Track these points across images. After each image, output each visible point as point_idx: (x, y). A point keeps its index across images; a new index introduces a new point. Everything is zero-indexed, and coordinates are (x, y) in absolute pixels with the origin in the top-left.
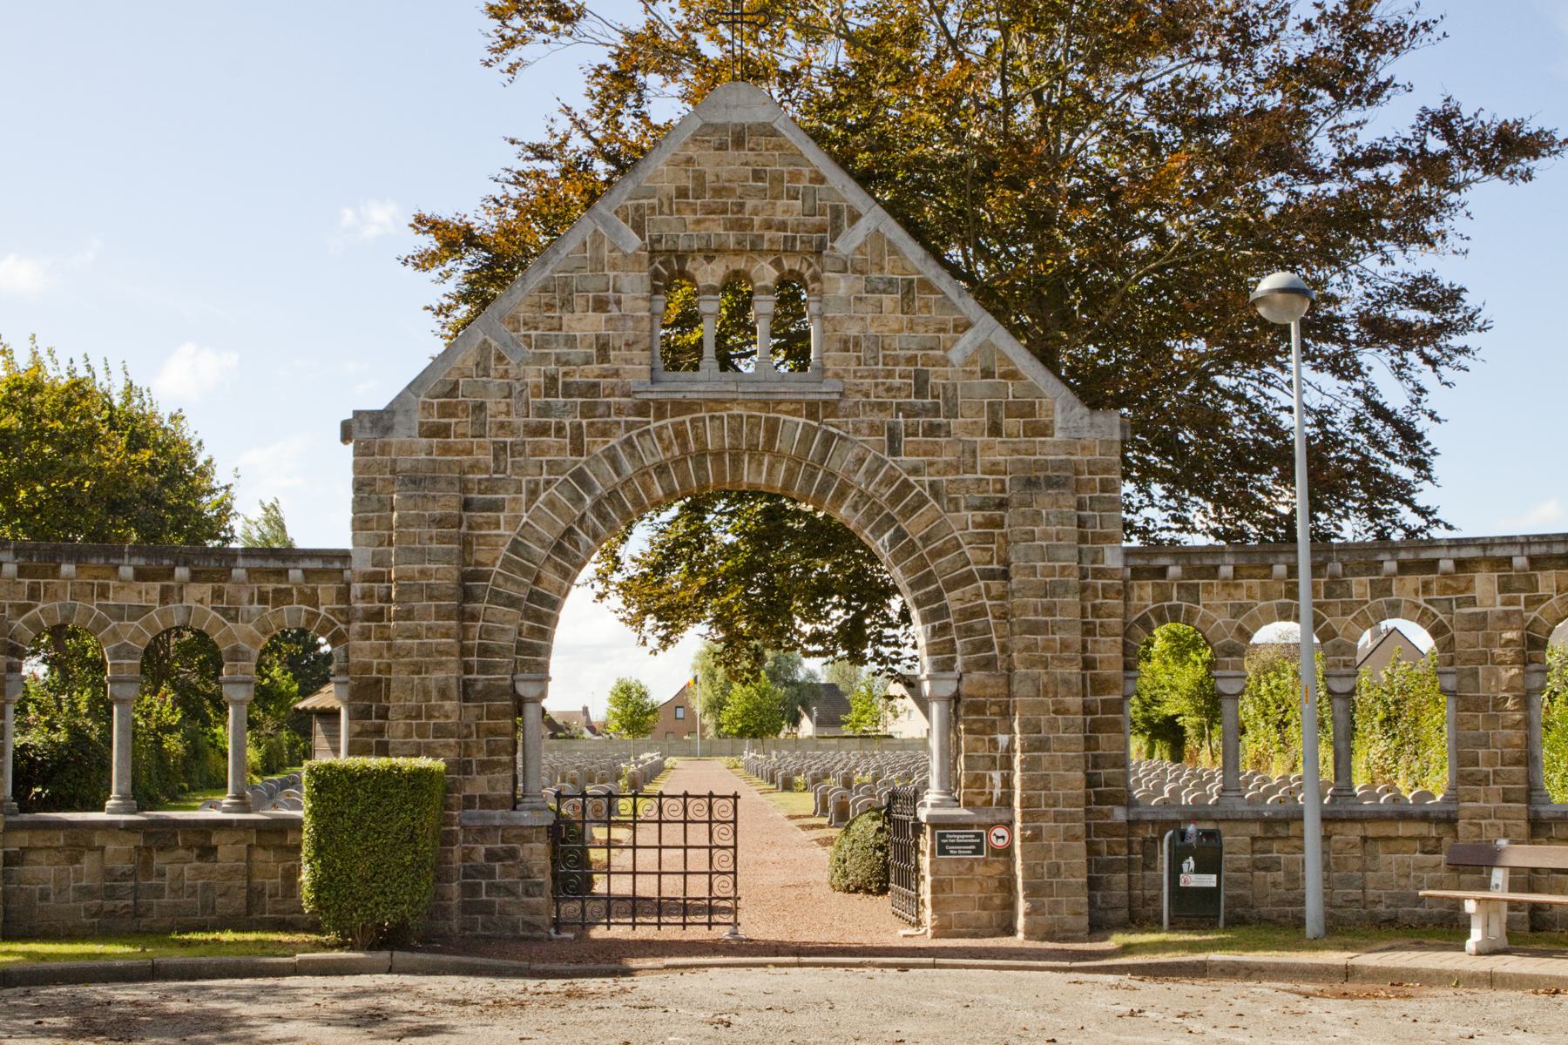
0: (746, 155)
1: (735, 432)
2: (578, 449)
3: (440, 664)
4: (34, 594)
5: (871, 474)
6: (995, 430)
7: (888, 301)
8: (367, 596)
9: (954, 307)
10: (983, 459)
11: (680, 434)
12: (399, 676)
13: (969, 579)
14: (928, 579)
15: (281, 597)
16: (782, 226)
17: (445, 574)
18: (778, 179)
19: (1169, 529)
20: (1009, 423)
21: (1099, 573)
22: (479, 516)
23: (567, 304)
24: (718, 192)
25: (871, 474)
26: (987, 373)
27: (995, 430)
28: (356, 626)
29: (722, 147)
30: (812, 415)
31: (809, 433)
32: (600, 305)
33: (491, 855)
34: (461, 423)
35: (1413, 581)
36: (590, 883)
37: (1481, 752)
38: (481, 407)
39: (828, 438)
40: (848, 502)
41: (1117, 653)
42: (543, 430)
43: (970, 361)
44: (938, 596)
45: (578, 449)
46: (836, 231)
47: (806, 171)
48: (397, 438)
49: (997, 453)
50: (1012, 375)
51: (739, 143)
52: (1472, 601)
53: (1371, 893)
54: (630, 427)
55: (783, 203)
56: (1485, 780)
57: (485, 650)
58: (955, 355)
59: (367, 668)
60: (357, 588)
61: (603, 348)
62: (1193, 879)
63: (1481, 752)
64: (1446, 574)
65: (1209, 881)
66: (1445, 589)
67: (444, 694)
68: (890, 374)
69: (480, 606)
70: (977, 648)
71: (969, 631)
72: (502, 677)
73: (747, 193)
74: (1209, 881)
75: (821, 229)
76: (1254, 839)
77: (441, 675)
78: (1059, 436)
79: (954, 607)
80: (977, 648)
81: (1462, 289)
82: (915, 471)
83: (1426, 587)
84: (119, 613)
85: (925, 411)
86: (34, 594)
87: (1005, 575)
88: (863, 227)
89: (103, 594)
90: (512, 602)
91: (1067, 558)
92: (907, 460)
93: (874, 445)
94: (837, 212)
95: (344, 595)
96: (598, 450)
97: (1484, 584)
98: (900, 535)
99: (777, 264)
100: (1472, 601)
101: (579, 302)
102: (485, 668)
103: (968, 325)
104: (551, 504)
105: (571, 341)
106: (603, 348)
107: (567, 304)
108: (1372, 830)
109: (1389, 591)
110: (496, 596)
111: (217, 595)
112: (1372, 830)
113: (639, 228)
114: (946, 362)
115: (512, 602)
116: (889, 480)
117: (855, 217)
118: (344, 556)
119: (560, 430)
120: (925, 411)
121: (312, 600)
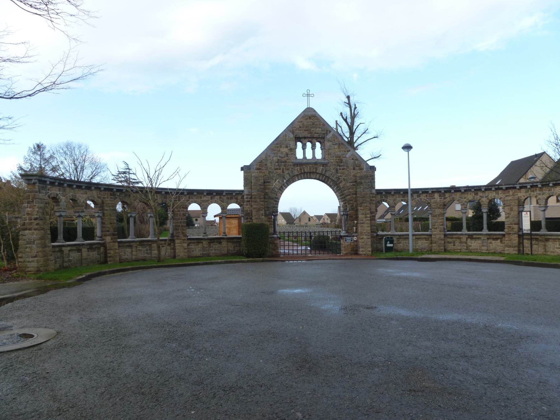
0: (311, 120)
4: (189, 198)
6: (354, 169)
7: (336, 147)
8: (247, 198)
11: (301, 169)
12: (254, 213)
14: (343, 194)
18: (317, 125)
19: (29, 262)
24: (307, 127)
26: (353, 159)
28: (245, 203)
30: (323, 166)
32: (287, 147)
35: (425, 195)
38: (266, 165)
39: (326, 171)
43: (350, 157)
45: (283, 172)
46: (327, 134)
48: (252, 170)
51: (310, 118)
52: (434, 198)
53: (417, 247)
54: (292, 168)
55: (318, 129)
56: (436, 228)
58: (347, 156)
59: (247, 211)
60: (245, 197)
62: (389, 245)
65: (392, 245)
66: (430, 196)
67: (262, 215)
73: (311, 128)
74: (392, 245)
75: (324, 134)
81: (242, 169)
83: (426, 196)
87: (356, 194)
89: (201, 198)
94: (327, 131)
95: (243, 198)
100: (434, 198)
102: (268, 210)
105: (282, 153)
107: (281, 147)
108: (417, 237)
112: (417, 237)
114: (346, 157)
118: (242, 191)
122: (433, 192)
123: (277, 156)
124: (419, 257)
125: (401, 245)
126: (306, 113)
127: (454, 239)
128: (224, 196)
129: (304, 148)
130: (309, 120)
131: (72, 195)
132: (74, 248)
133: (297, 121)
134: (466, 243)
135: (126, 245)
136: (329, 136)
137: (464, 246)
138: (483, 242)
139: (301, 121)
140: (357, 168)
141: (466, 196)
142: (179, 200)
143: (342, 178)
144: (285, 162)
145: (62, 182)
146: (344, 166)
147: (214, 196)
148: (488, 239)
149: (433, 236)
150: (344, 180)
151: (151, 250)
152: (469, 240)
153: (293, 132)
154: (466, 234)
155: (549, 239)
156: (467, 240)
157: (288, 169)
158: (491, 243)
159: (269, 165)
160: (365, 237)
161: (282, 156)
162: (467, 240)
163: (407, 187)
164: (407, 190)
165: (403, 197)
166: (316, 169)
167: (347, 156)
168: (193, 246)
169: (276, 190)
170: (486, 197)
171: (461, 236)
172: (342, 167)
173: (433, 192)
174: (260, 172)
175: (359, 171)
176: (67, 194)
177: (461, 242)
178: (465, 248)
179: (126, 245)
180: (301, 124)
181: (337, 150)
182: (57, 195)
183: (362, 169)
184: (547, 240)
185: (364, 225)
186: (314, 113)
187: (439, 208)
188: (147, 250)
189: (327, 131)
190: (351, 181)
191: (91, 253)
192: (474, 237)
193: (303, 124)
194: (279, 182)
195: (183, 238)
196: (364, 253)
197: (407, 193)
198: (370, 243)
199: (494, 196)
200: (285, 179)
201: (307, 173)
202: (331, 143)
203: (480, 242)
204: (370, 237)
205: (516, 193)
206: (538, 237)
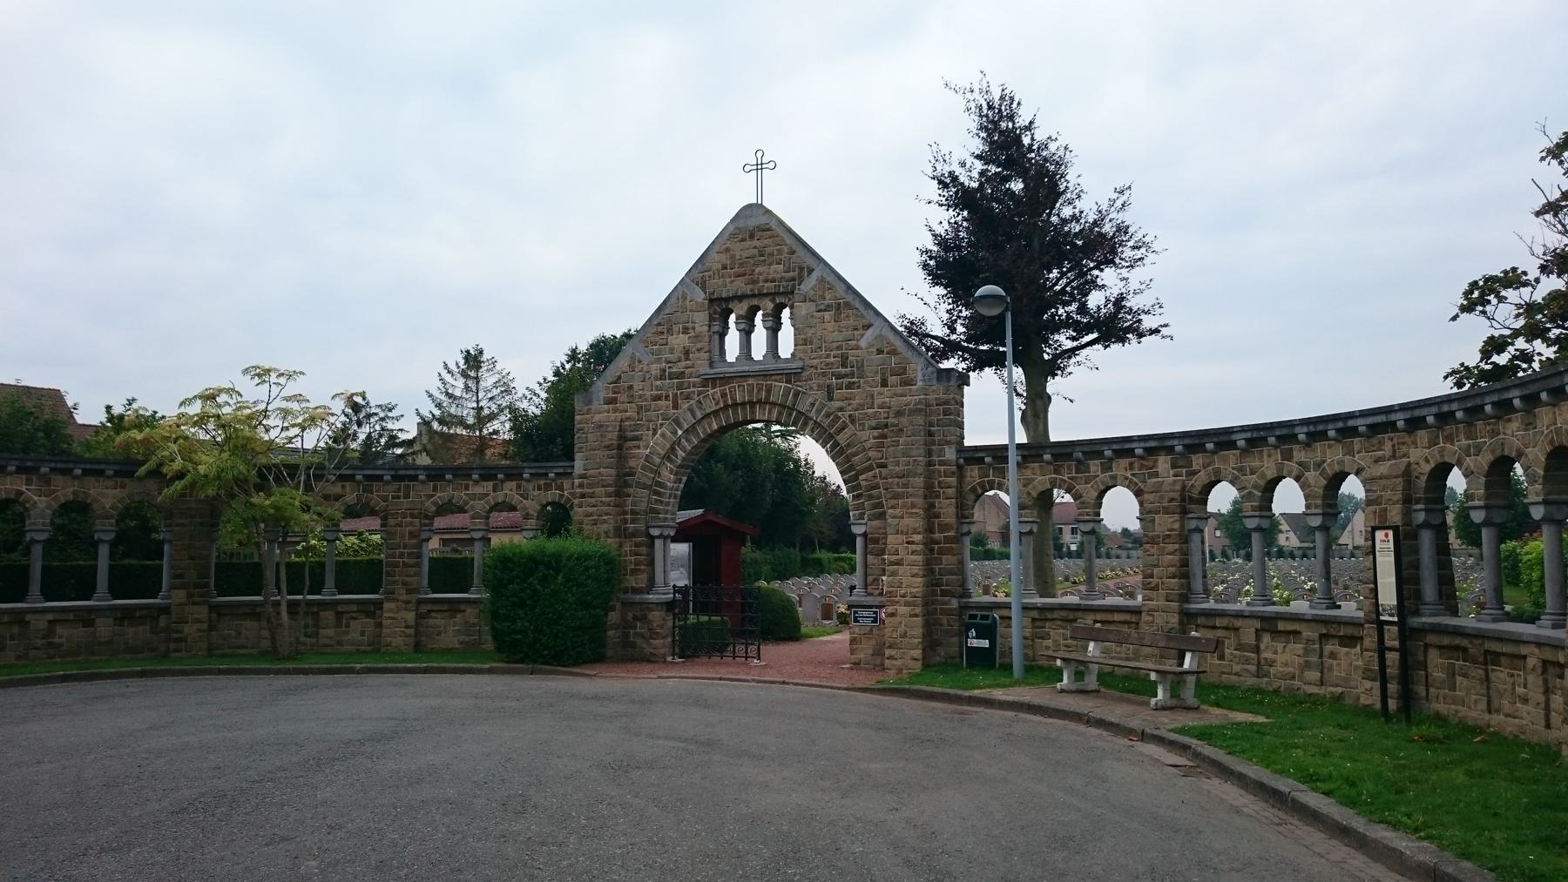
0: (755, 243)
1: (750, 392)
2: (676, 407)
3: (605, 522)
4: (435, 489)
5: (819, 411)
6: (884, 383)
7: (827, 315)
8: (581, 486)
9: (862, 316)
10: (878, 401)
11: (724, 395)
13: (870, 468)
14: (851, 468)
15: (548, 487)
16: (773, 281)
17: (609, 474)
20: (892, 380)
21: (942, 463)
22: (630, 444)
23: (670, 331)
24: (741, 265)
25: (819, 411)
26: (880, 352)
27: (884, 383)
29: (743, 240)
31: (787, 391)
32: (686, 331)
33: (635, 618)
34: (622, 397)
35: (1124, 462)
36: (1528, 515)
37: (1156, 571)
38: (631, 387)
39: (796, 394)
40: (105, 532)
41: (952, 510)
42: (658, 398)
44: (856, 477)
45: (676, 407)
47: (786, 249)
49: (884, 396)
50: (894, 352)
51: (752, 236)
52: (1157, 475)
57: (633, 512)
58: (863, 343)
60: (577, 482)
61: (687, 353)
63: (1156, 571)
64: (1141, 458)
65: (985, 643)
66: (1142, 467)
68: (828, 356)
69: (631, 490)
70: (875, 506)
71: (870, 497)
72: (641, 526)
74: (985, 643)
75: (793, 279)
76: (1034, 620)
77: (605, 526)
78: (920, 384)
79: (863, 483)
80: (875, 506)
82: (841, 409)
83: (1131, 464)
84: (473, 497)
85: (846, 376)
86: (435, 489)
88: (815, 275)
89: (467, 488)
90: (645, 487)
91: (919, 454)
92: (838, 404)
93: (820, 395)
94: (801, 269)
96: (686, 406)
97: (1163, 463)
98: (836, 444)
99: (773, 300)
100: (1157, 475)
101: (675, 328)
103: (869, 326)
104: (663, 435)
106: (687, 353)
107: (670, 331)
109: (1110, 469)
110: (639, 485)
111: (519, 487)
113: (704, 289)
114: (858, 348)
115: (645, 487)
116: (828, 415)
117: (811, 271)
119: (667, 397)
120: (846, 376)
121: (561, 488)
122: (1150, 451)
123: (659, 361)
124: (967, 693)
125: (1049, 643)
126: (741, 224)
127: (1220, 633)
128: (528, 481)
129: (747, 332)
130: (748, 243)
131: (74, 493)
132: (446, 607)
133: (717, 248)
134: (1257, 650)
135: (241, 611)
136: (808, 285)
137: (1247, 661)
138: (1307, 652)
139: (727, 250)
140: (892, 380)
141: (1256, 464)
142: (407, 496)
143: (844, 417)
144: (681, 375)
145: (1445, 408)
146: (852, 375)
147: (502, 481)
148: (1324, 638)
149: (1145, 617)
150: (852, 420)
151: (317, 626)
152: (1266, 638)
153: (703, 285)
154: (1252, 616)
155: (1499, 654)
156: (1258, 638)
157: (688, 397)
158: (1333, 655)
159: (637, 385)
160: (902, 609)
161: (673, 357)
162: (1258, 638)
163: (1006, 442)
164: (1004, 448)
165: (1056, 471)
166: (769, 391)
167: (863, 343)
168: (437, 621)
169: (657, 460)
170: (1319, 465)
171: (1238, 623)
172: (846, 380)
173: (1150, 451)
174: (615, 411)
175: (900, 390)
176: (55, 491)
177: (1240, 647)
178: (1253, 668)
179: (241, 611)
180: (724, 258)
181: (830, 326)
182: (20, 493)
183: (909, 383)
184: (1492, 658)
185: (901, 569)
186: (763, 220)
187: (1167, 511)
188: (306, 626)
189: (801, 269)
190: (873, 423)
191: (130, 631)
192: (1281, 626)
193: (732, 257)
194: (663, 435)
195: (405, 597)
196: (898, 663)
197: (1005, 459)
198: (919, 631)
199: (1341, 462)
200: (679, 425)
201: (743, 404)
202: (811, 307)
203: (1299, 647)
204: (918, 610)
205: (1404, 449)
206: (1465, 642)
